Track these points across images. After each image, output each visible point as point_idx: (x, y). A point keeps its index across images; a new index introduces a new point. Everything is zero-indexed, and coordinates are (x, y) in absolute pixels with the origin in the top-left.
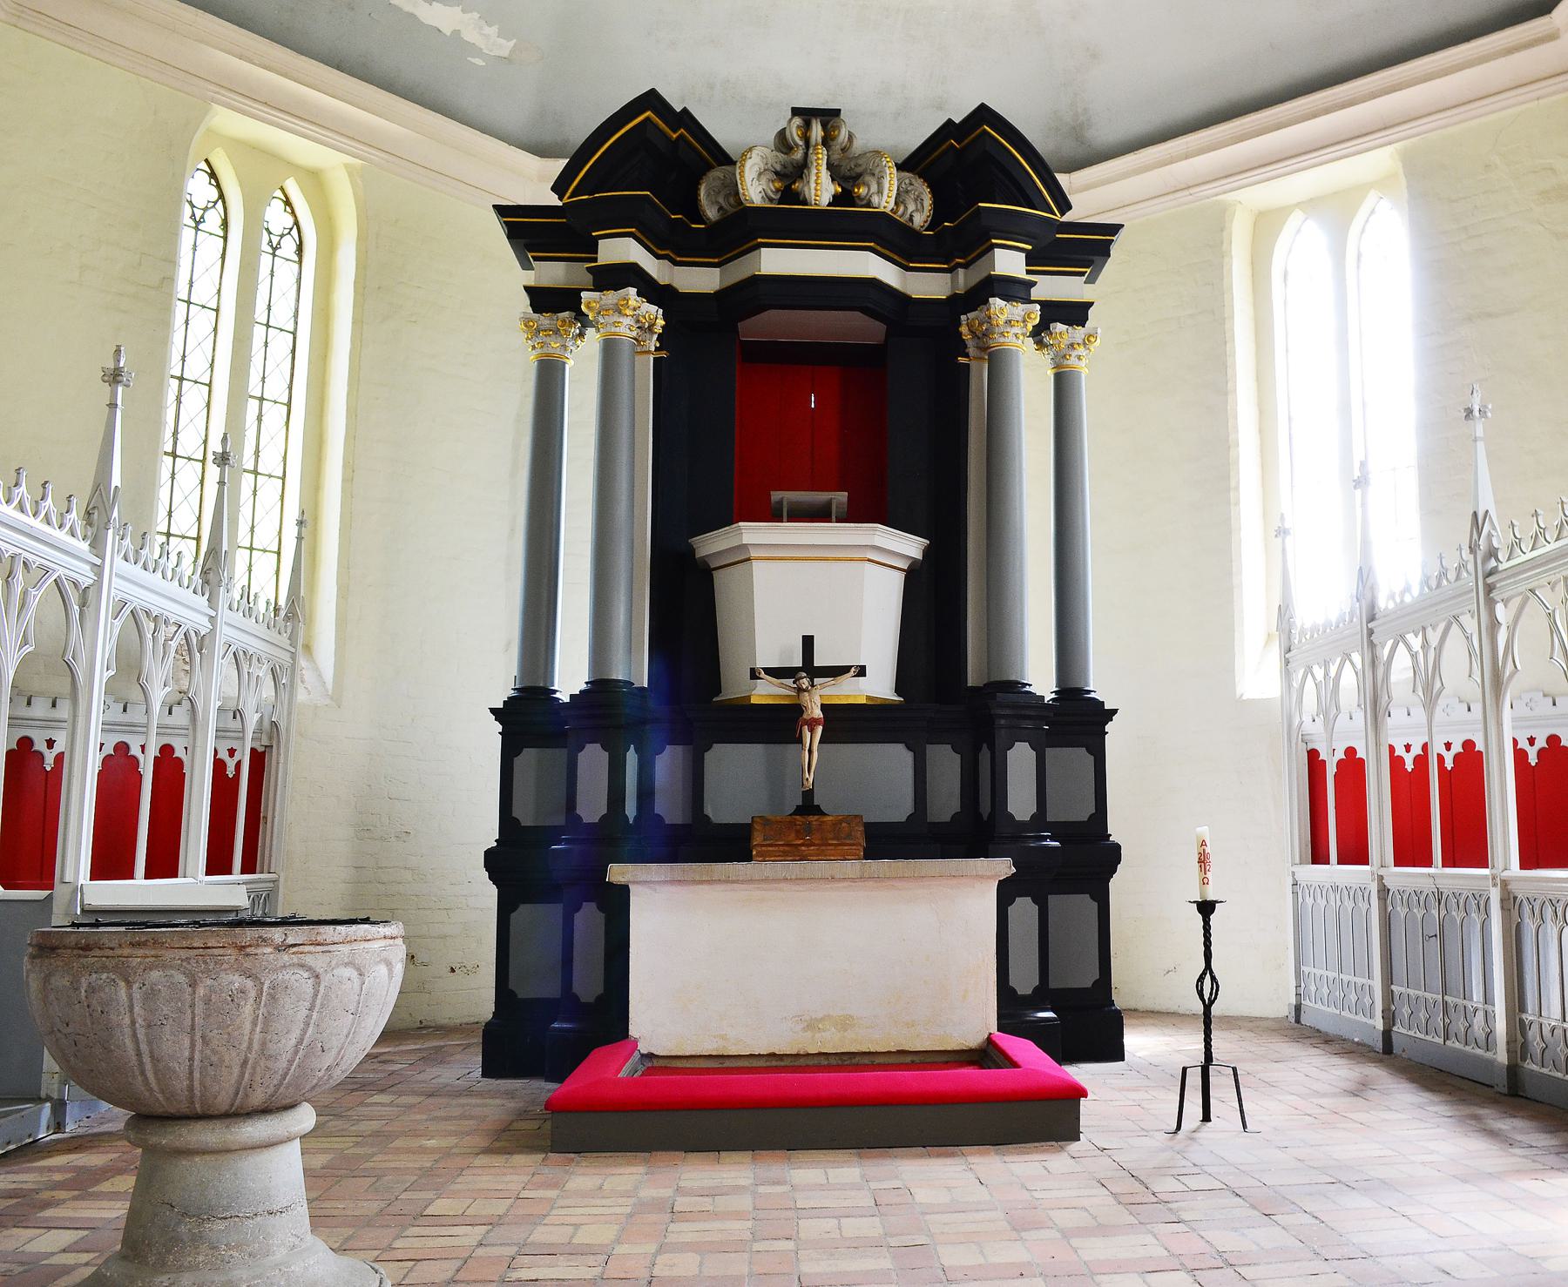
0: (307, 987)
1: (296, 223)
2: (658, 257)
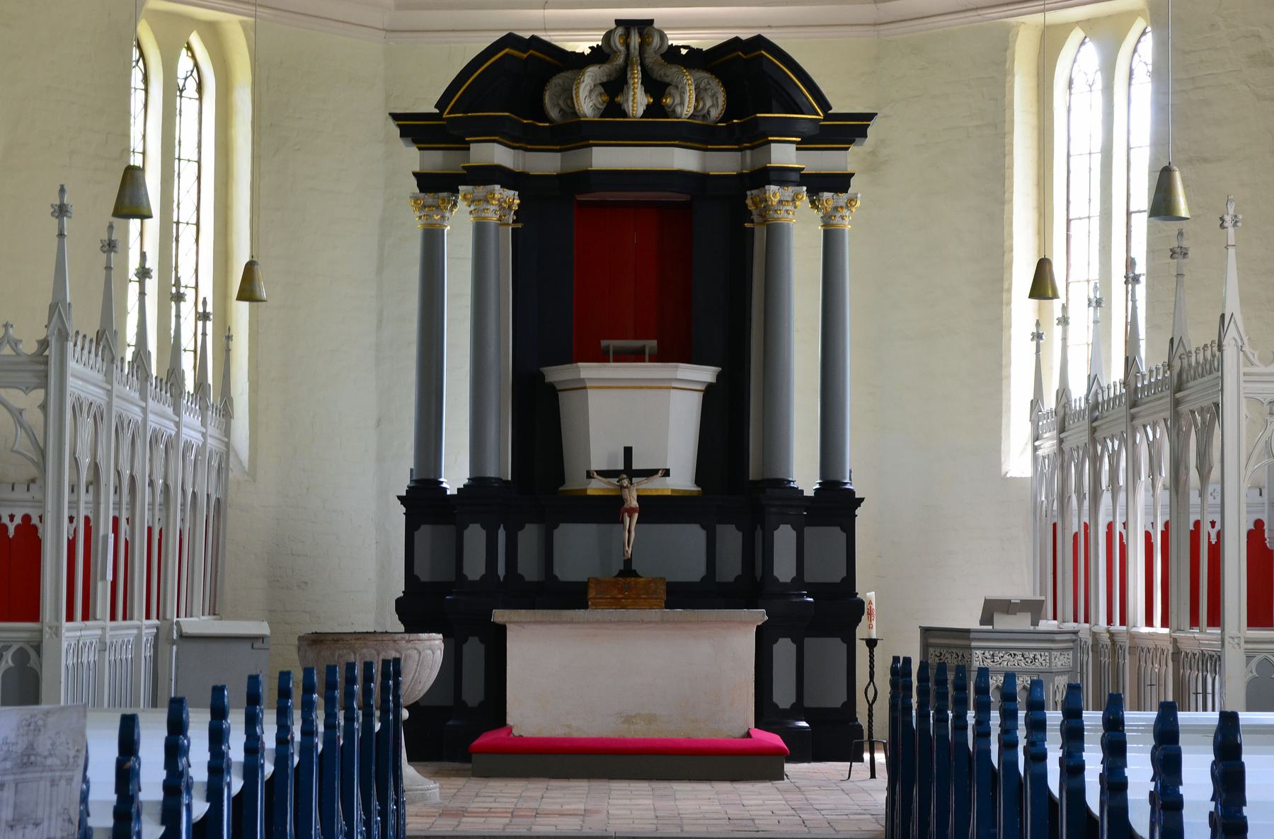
0: (417, 657)
1: (196, 65)
2: (513, 148)
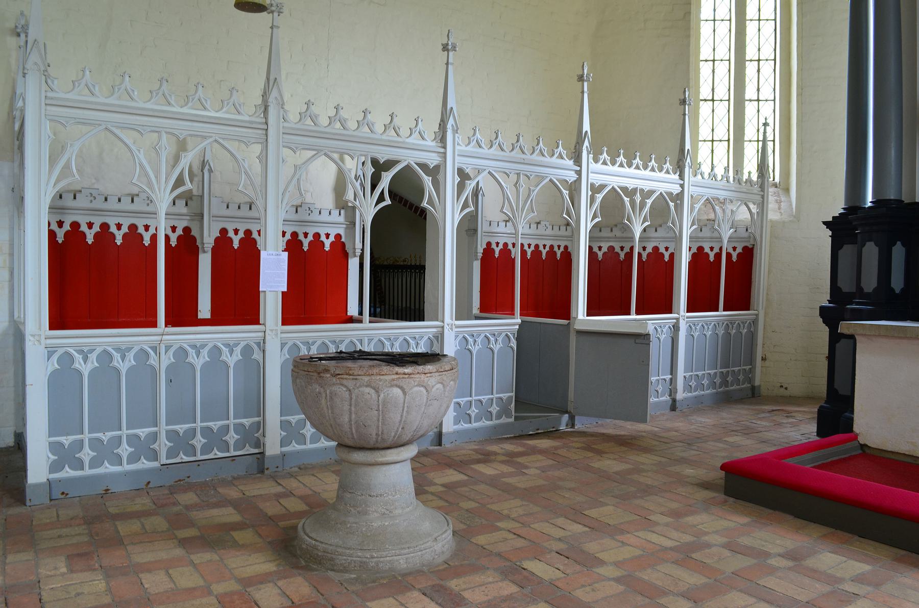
0: (347, 395)
